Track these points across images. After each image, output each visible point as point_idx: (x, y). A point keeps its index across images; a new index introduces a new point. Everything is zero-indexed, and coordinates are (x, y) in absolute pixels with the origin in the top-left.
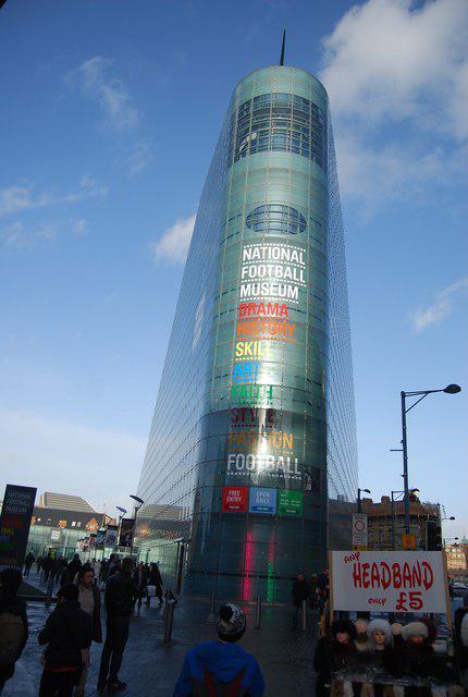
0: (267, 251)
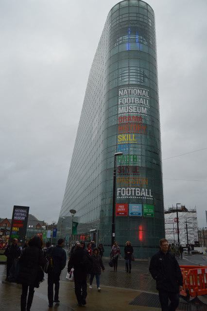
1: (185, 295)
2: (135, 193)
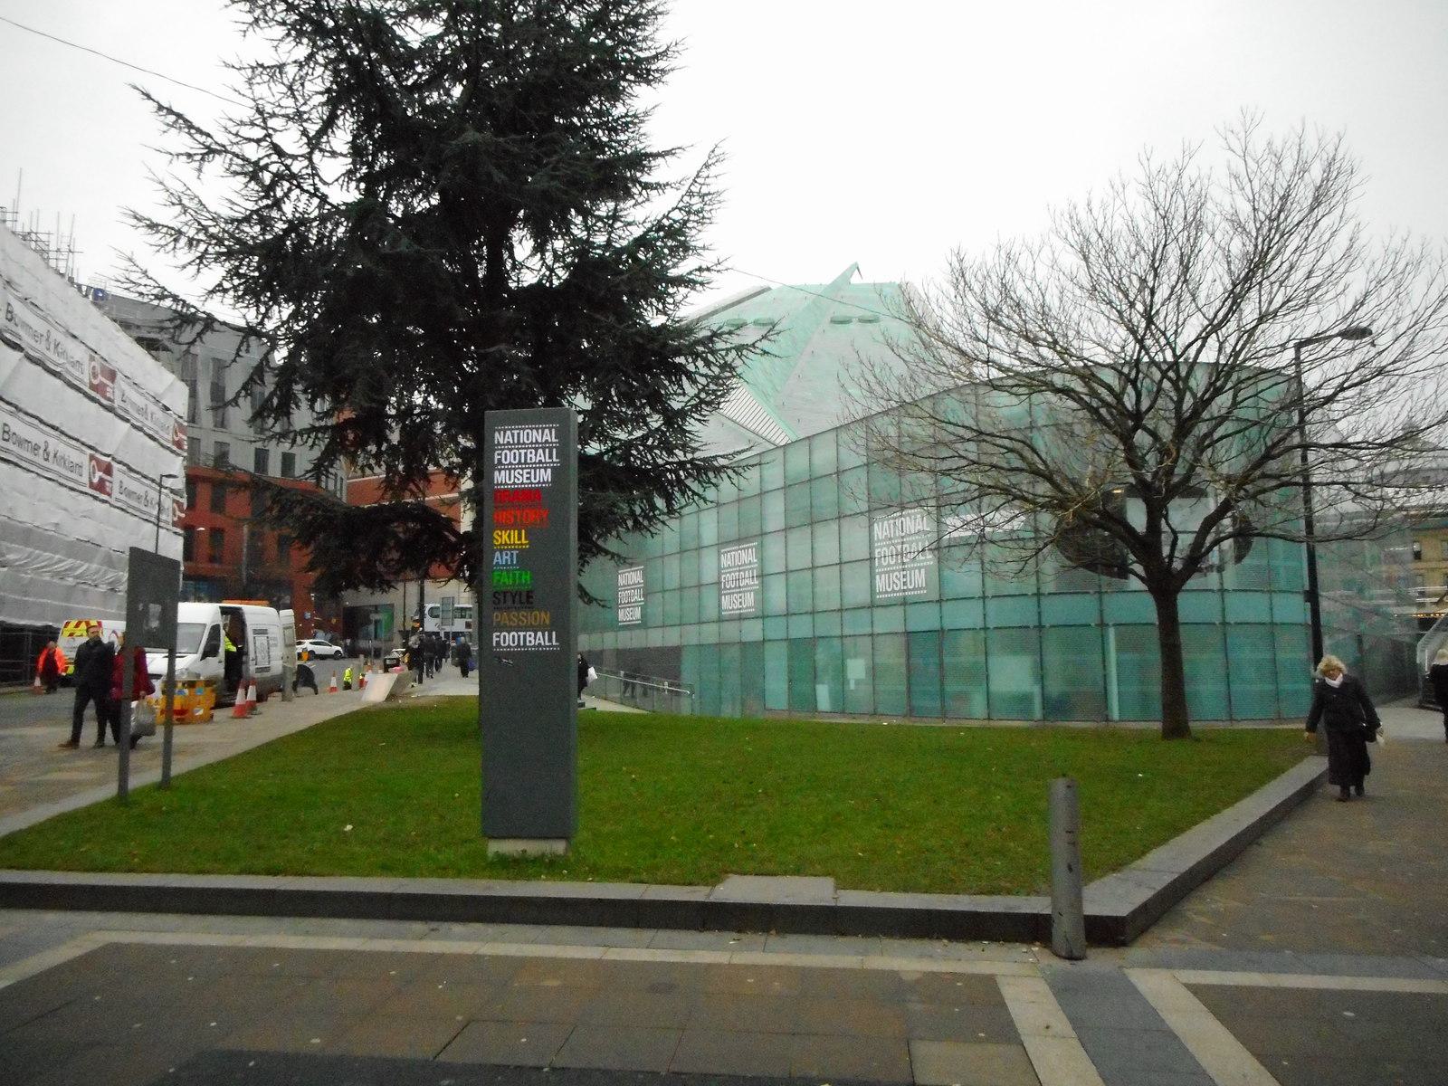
0: (519, 434)
2: (525, 642)
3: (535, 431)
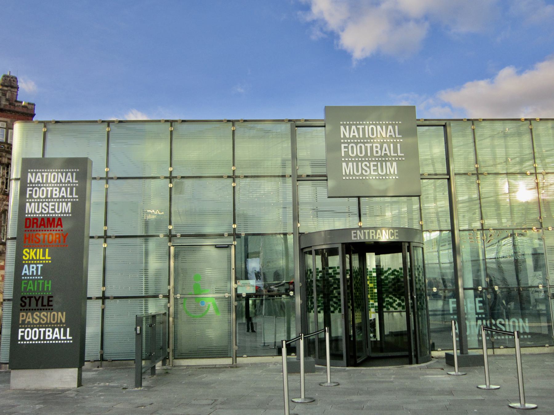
1: (336, 295)
3: (378, 127)
